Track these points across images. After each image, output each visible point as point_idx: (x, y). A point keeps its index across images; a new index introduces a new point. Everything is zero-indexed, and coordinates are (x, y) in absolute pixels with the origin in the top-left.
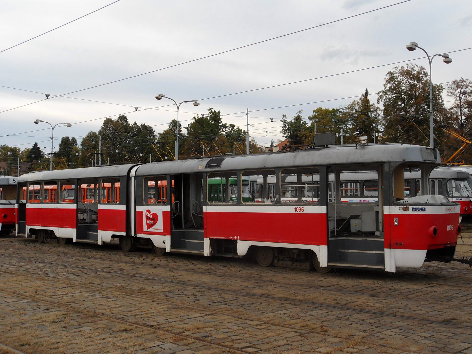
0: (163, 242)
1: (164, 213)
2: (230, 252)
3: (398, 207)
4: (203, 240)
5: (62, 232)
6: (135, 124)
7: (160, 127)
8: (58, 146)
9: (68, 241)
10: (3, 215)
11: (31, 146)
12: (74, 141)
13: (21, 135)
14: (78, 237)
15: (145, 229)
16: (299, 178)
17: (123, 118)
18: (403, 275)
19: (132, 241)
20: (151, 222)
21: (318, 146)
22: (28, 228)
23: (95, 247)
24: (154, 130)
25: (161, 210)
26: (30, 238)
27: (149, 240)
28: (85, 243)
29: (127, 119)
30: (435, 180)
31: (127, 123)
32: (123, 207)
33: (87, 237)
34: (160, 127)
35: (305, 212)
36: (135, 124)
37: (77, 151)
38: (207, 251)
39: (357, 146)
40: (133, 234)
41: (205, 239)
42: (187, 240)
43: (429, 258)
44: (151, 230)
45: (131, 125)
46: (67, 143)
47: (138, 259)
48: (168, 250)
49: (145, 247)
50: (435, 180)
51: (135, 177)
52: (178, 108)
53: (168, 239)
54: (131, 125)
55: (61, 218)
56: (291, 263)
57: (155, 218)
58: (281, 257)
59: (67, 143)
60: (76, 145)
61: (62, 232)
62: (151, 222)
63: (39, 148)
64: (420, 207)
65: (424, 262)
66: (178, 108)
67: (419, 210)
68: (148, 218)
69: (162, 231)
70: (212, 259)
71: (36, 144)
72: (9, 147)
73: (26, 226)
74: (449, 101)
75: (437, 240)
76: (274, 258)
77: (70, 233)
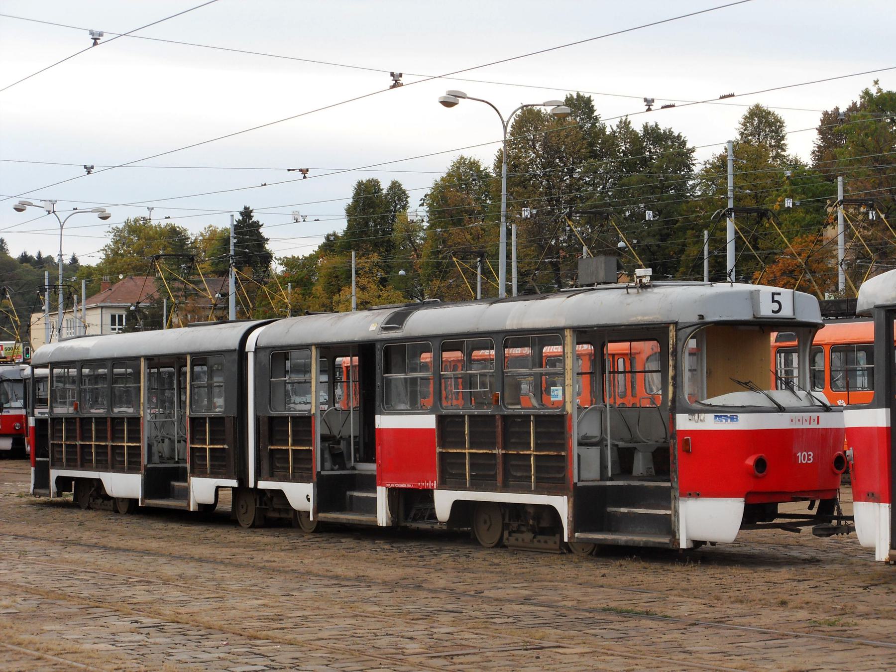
2: (422, 518)
4: (375, 491)
6: (625, 124)
7: (709, 136)
8: (344, 213)
10: (750, 461)
11: (225, 222)
12: (398, 193)
14: (318, 508)
17: (581, 105)
19: (256, 500)
21: (605, 283)
22: (54, 474)
23: (183, 516)
24: (689, 146)
26: (59, 499)
27: (280, 493)
28: (161, 502)
29: (591, 110)
31: (594, 125)
33: (168, 493)
34: (709, 136)
36: (625, 124)
37: (411, 229)
38: (382, 517)
39: (627, 288)
40: (251, 485)
41: (379, 488)
42: (356, 494)
43: (749, 520)
45: (608, 131)
46: (373, 207)
47: (263, 538)
51: (255, 352)
54: (608, 131)
56: (531, 535)
58: (515, 525)
59: (373, 207)
60: (405, 207)
63: (257, 225)
64: (729, 415)
65: (740, 529)
67: (726, 421)
70: (394, 534)
71: (247, 213)
75: (792, 483)
76: (505, 527)
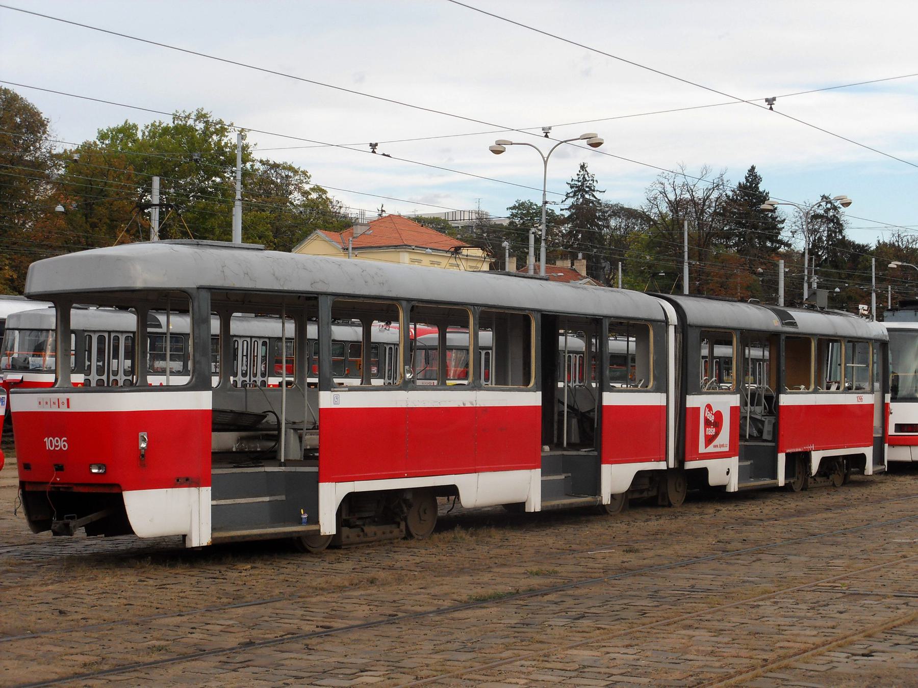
0: (725, 472)
1: (733, 409)
3: (856, 395)
5: (479, 489)
9: (511, 516)
13: (872, 225)
15: (702, 449)
16: (443, 338)
18: (172, 553)
20: (711, 431)
25: (726, 402)
28: (575, 510)
30: (92, 335)
32: (693, 401)
35: (73, 409)
44: (711, 449)
48: (733, 487)
49: (699, 489)
50: (92, 335)
52: (545, 163)
53: (734, 463)
55: (169, 451)
57: (717, 423)
61: (479, 489)
62: (711, 431)
66: (545, 163)
68: (708, 423)
69: (727, 449)
72: (698, 206)
73: (606, 469)
74: (296, 198)
77: (525, 486)
